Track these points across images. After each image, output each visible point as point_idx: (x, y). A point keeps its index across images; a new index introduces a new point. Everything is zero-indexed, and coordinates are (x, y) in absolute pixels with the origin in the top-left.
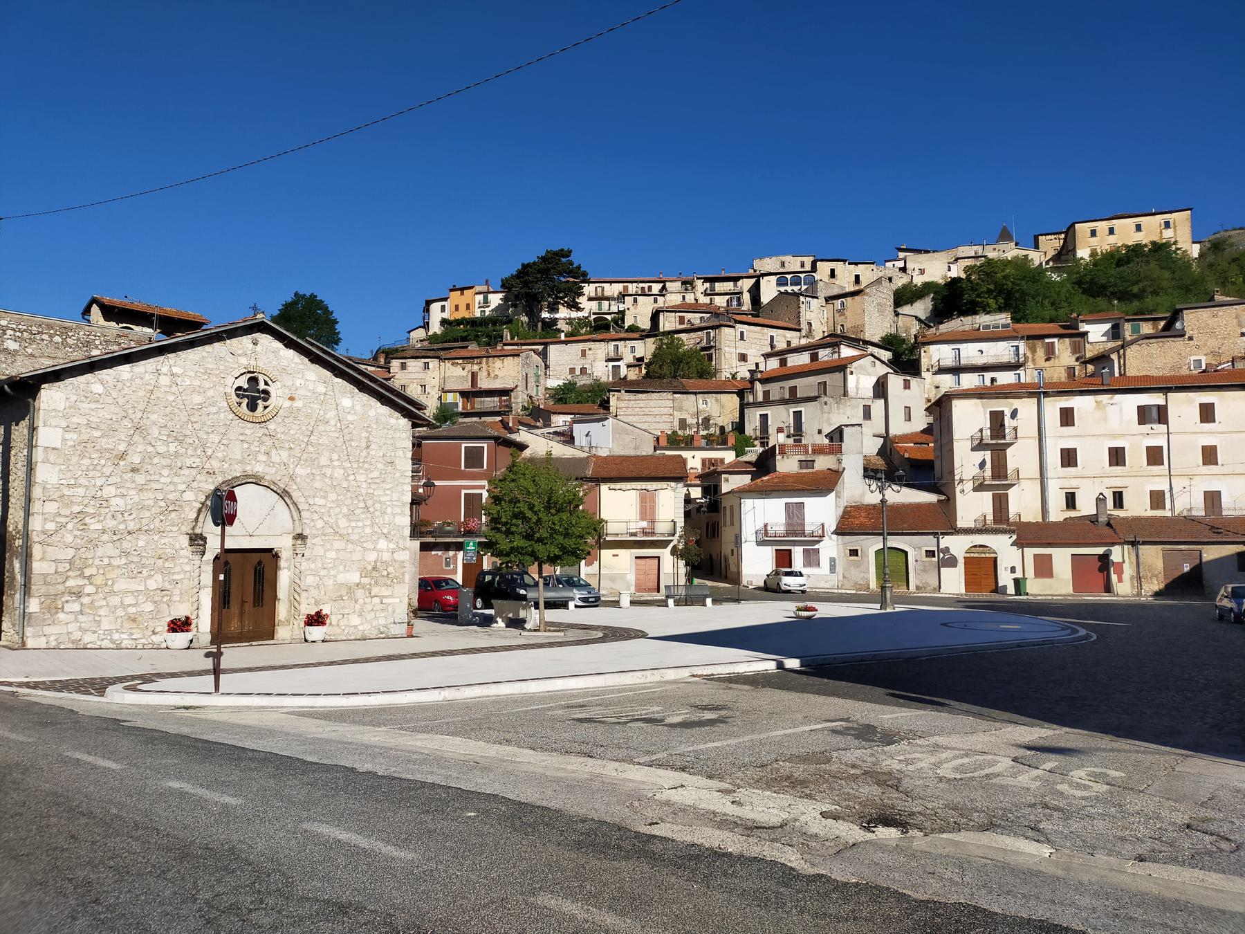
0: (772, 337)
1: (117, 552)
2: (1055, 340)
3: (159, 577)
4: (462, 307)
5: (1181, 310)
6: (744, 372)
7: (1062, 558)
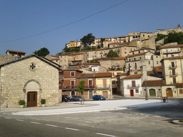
0: (131, 49)
3: (19, 96)
4: (73, 45)
6: (126, 55)
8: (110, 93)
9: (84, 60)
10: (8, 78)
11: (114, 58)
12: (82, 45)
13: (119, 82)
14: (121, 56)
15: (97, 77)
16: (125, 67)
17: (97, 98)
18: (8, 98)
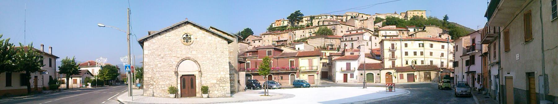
1: (160, 76)
2: (404, 31)
3: (168, 81)
5: (425, 27)
6: (342, 34)
7: (405, 75)
8: (317, 77)
9: (290, 40)
10: (153, 57)
11: (328, 36)
12: (289, 24)
13: (331, 64)
14: (336, 34)
15: (300, 56)
16: (340, 47)
17: (298, 85)
18: (154, 84)
